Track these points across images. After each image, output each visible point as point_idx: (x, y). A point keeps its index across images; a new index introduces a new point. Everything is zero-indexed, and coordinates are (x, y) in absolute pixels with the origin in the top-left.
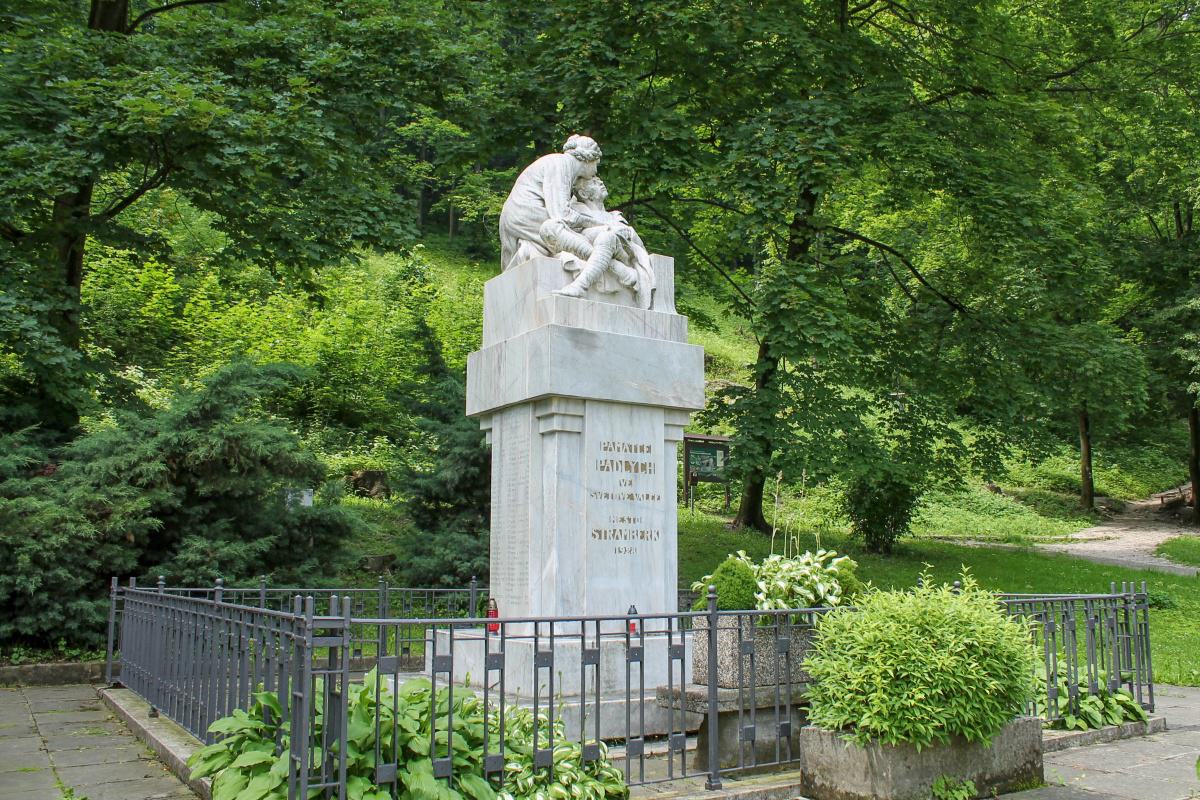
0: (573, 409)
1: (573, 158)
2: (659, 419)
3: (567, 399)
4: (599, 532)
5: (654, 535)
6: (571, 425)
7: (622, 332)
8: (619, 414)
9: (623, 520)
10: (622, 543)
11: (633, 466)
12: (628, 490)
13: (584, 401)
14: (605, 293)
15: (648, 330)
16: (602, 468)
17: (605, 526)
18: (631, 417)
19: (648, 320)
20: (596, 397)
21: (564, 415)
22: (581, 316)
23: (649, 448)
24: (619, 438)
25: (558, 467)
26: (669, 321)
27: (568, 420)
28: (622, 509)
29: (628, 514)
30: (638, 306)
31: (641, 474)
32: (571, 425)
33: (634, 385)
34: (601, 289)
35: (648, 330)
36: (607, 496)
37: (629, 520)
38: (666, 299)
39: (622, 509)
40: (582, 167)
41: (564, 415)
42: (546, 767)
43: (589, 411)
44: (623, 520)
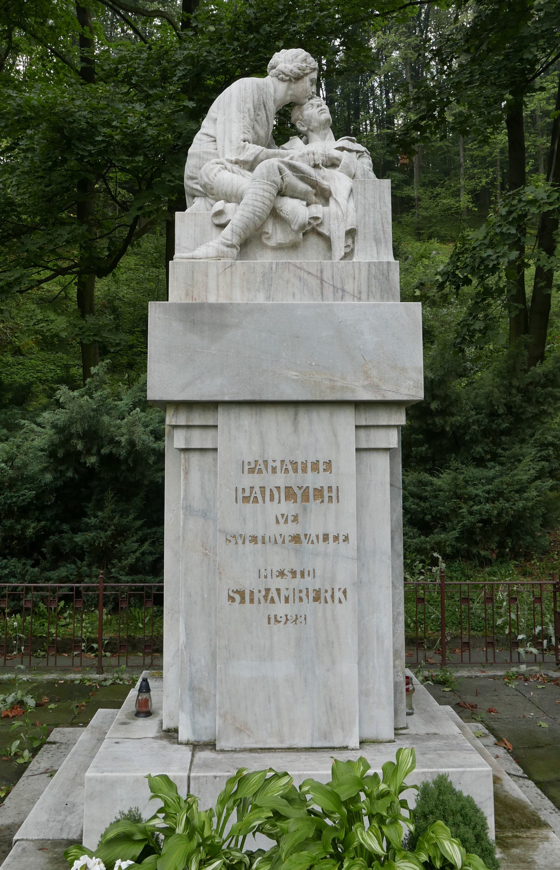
0: (197, 419)
1: (275, 79)
2: (346, 420)
3: (189, 405)
4: (241, 593)
5: (338, 595)
6: (198, 439)
7: (283, 298)
8: (273, 420)
9: (281, 574)
10: (281, 609)
11: (299, 493)
12: (291, 529)
13: (212, 406)
14: (280, 248)
15: (328, 291)
16: (246, 499)
17: (250, 582)
18: (296, 415)
19: (327, 276)
20: (227, 398)
21: (188, 427)
22: (212, 284)
23: (329, 464)
24: (275, 453)
25: (186, 498)
26: (364, 273)
27: (196, 434)
28: (279, 558)
29: (293, 563)
30: (330, 258)
31: (314, 505)
32: (198, 439)
33: (292, 374)
34: (272, 243)
35: (328, 291)
36: (254, 539)
37: (294, 573)
38: (377, 241)
39: (279, 558)
40: (289, 88)
41: (188, 427)
42: (361, 791)
43: (222, 418)
44: (281, 574)
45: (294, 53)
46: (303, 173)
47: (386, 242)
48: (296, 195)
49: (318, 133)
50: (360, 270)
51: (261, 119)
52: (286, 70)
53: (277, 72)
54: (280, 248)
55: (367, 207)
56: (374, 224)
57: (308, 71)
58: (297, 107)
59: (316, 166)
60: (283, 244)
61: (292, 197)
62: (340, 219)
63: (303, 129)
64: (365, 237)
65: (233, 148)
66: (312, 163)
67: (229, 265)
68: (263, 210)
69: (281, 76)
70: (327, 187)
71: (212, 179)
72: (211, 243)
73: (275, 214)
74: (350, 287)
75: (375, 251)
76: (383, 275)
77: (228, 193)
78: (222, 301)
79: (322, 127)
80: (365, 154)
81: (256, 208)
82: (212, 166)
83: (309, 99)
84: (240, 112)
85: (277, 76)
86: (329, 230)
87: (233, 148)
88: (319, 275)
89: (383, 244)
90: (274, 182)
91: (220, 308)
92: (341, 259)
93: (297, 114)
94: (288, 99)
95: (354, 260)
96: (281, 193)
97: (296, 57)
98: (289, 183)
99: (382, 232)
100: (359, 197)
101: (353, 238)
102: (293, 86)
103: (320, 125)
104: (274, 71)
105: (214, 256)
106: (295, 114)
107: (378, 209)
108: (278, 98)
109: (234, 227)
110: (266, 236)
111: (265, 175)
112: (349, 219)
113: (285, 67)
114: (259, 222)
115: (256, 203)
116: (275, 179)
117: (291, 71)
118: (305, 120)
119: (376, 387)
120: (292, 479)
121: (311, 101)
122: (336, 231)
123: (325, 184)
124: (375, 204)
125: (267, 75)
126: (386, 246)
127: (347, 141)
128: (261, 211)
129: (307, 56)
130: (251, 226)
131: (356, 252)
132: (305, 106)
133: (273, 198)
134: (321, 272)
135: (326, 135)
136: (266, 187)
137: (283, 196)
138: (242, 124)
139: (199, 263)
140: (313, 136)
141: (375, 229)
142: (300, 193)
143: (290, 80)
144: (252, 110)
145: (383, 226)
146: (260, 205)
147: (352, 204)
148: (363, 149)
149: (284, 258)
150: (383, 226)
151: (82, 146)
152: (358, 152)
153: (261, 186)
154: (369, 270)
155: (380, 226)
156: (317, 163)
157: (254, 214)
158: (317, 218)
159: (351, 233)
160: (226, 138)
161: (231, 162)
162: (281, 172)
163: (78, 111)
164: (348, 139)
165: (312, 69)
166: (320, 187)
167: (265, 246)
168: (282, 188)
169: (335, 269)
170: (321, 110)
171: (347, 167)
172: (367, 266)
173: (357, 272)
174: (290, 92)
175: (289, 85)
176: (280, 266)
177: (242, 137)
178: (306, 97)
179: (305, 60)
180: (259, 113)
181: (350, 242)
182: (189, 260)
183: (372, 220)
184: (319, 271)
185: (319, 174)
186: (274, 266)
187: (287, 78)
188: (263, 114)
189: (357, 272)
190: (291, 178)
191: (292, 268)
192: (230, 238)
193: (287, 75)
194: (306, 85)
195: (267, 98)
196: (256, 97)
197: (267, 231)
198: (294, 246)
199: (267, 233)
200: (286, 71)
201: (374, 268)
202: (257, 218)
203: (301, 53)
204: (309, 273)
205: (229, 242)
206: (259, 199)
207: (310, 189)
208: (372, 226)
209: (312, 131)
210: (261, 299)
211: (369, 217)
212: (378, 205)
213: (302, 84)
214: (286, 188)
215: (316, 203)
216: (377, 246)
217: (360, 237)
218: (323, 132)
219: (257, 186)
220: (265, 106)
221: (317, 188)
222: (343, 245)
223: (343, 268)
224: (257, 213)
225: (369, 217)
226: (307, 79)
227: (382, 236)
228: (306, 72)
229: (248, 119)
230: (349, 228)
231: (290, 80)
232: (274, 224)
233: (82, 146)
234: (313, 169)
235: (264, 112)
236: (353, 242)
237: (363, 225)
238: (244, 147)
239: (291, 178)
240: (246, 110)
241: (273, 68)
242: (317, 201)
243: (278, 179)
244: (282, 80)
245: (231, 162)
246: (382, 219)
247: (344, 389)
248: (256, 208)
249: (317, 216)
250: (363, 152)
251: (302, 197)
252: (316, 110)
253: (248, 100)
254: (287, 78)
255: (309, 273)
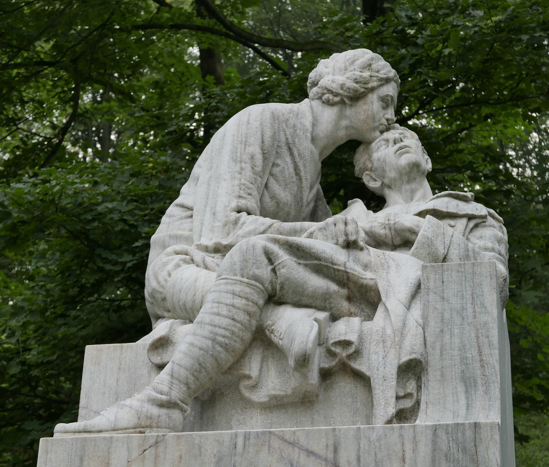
1: (316, 104)
14: (276, 405)
34: (260, 396)
38: (469, 383)
40: (341, 117)
45: (348, 57)
46: (317, 258)
47: (487, 384)
48: (305, 301)
49: (400, 190)
50: (415, 441)
51: (282, 172)
52: (334, 85)
53: (320, 90)
54: (276, 405)
55: (447, 316)
56: (462, 348)
57: (375, 84)
58: (361, 148)
59: (350, 245)
60: (282, 397)
61: (298, 305)
62: (389, 343)
63: (373, 185)
64: (442, 376)
65: (218, 224)
66: (341, 240)
67: (152, 441)
68: (233, 333)
69: (326, 96)
70: (371, 283)
71: (163, 283)
72: (128, 402)
73: (261, 338)
75: (463, 401)
76: (464, 450)
77: (189, 305)
79: (405, 178)
80: (490, 220)
81: (217, 330)
82: (165, 259)
83: (382, 132)
84: (235, 161)
85: (320, 98)
86: (369, 368)
87: (218, 224)
88: (330, 455)
89: (481, 390)
90: (256, 278)
92: (390, 422)
93: (362, 160)
94: (342, 136)
95: (418, 422)
96: (274, 299)
97: (353, 62)
98: (288, 279)
99: (478, 365)
100: (432, 297)
101: (419, 379)
102: (349, 112)
103: (401, 174)
104: (315, 89)
105: (131, 424)
106: (360, 159)
107: (470, 319)
108: (321, 135)
109: (176, 368)
110: (247, 383)
111: (238, 267)
112: (407, 343)
113: (333, 81)
114: (227, 359)
115: (217, 320)
116: (257, 272)
117: (342, 86)
118: (376, 169)
121: (386, 135)
122: (380, 365)
123: (367, 276)
124: (463, 309)
126: (487, 392)
127: (447, 199)
128: (227, 333)
129: (372, 59)
130: (209, 363)
131: (423, 406)
132: (373, 145)
133: (253, 309)
134: (336, 450)
135: (413, 192)
136: (238, 288)
137: (280, 303)
138: (236, 182)
139: (95, 440)
140: (391, 196)
141: (464, 360)
142: (313, 296)
143: (342, 102)
144: (259, 158)
145: (480, 353)
146: (225, 322)
147: (416, 312)
148: (480, 209)
149: (287, 427)
150: (480, 353)
151: (114, 257)
152: (470, 217)
153: (230, 288)
154: (434, 443)
155: (475, 353)
156: (352, 238)
157: (214, 340)
158: (346, 344)
159: (412, 370)
160: (208, 209)
161: (206, 249)
162: (270, 257)
163: (103, 202)
164: (450, 195)
165: (381, 79)
166: (355, 283)
167: (248, 404)
168: (274, 289)
169: (364, 443)
170: (401, 148)
171: (429, 243)
172: (430, 433)
173: (408, 447)
174: (344, 123)
175: (341, 110)
176: (252, 441)
177: (234, 204)
178: (374, 129)
179: (369, 66)
180: (279, 161)
181: (411, 387)
182: (77, 436)
183: (456, 340)
184: (331, 448)
185: (357, 261)
186: (240, 442)
187: (337, 99)
188: (286, 164)
189: (408, 447)
190: (291, 268)
191: (276, 443)
192: (166, 389)
193: (336, 95)
195: (294, 135)
196: (268, 133)
197: (247, 372)
198: (303, 402)
199: (249, 377)
200: (335, 87)
201: (444, 437)
202: (219, 348)
203: (364, 55)
204: (310, 453)
205: (164, 397)
206: (224, 312)
207: (334, 287)
208: (456, 353)
209: (389, 187)
211: (452, 335)
212: (470, 310)
213: (365, 107)
214: (282, 288)
215: (351, 315)
216: (467, 392)
217: (432, 377)
218: (408, 187)
219: (222, 287)
220: (290, 149)
221: (351, 285)
222: (391, 394)
223: (379, 439)
224: (220, 339)
225: (452, 335)
226: (373, 98)
227: (479, 372)
228: (370, 85)
229: (248, 172)
230: (405, 358)
231: (342, 102)
232: (264, 360)
233: (114, 257)
234: (344, 251)
235: (288, 159)
236: (419, 388)
237: (438, 352)
238: (236, 222)
239: (291, 268)
240: (246, 157)
241: (315, 84)
242: (353, 309)
243: (265, 272)
244: (328, 103)
245: (206, 249)
246: (477, 337)
248: (217, 330)
249: (347, 338)
250: (484, 217)
251: (318, 303)
252: (397, 151)
253: (252, 140)
254: (337, 99)
255: (310, 453)
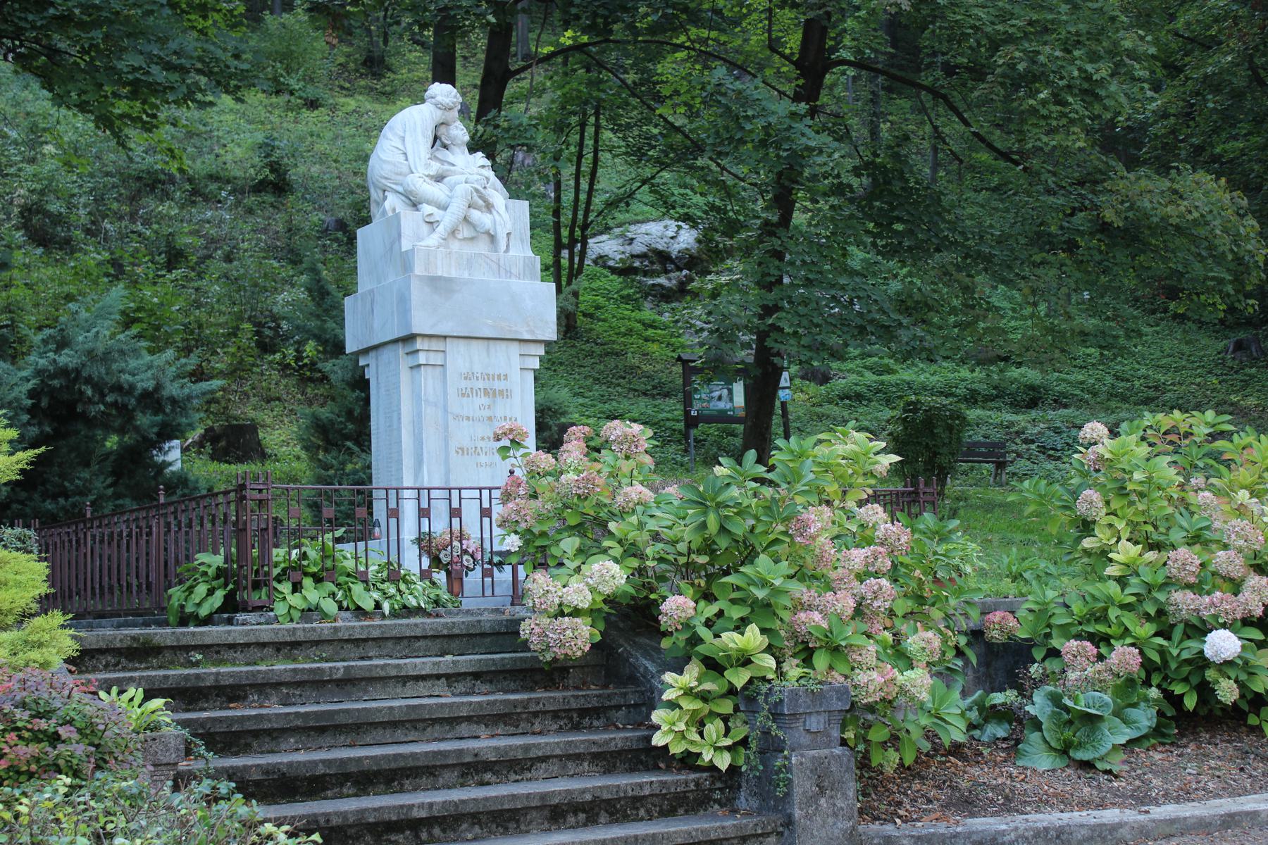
2: (515, 349)
4: (462, 449)
9: (483, 439)
12: (487, 413)
13: (445, 337)
15: (502, 272)
16: (463, 395)
17: (466, 443)
19: (502, 263)
30: (496, 251)
34: (460, 236)
35: (502, 272)
36: (468, 418)
38: (522, 241)
44: (483, 439)
74: (514, 271)
78: (445, 275)
91: (449, 280)
119: (532, 332)
120: (487, 384)
125: (423, 101)
159: (508, 234)
194: (455, 113)
210: (466, 276)
247: (516, 332)
